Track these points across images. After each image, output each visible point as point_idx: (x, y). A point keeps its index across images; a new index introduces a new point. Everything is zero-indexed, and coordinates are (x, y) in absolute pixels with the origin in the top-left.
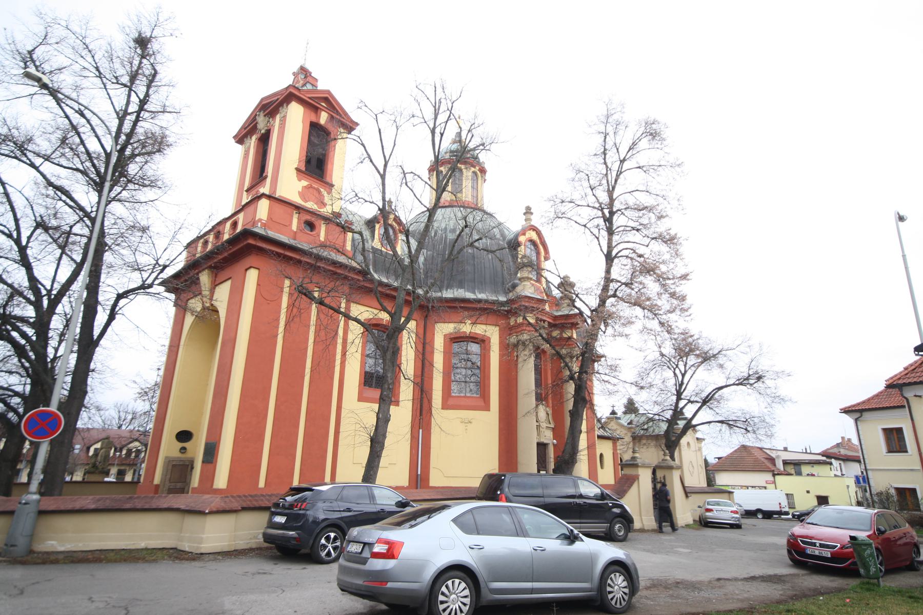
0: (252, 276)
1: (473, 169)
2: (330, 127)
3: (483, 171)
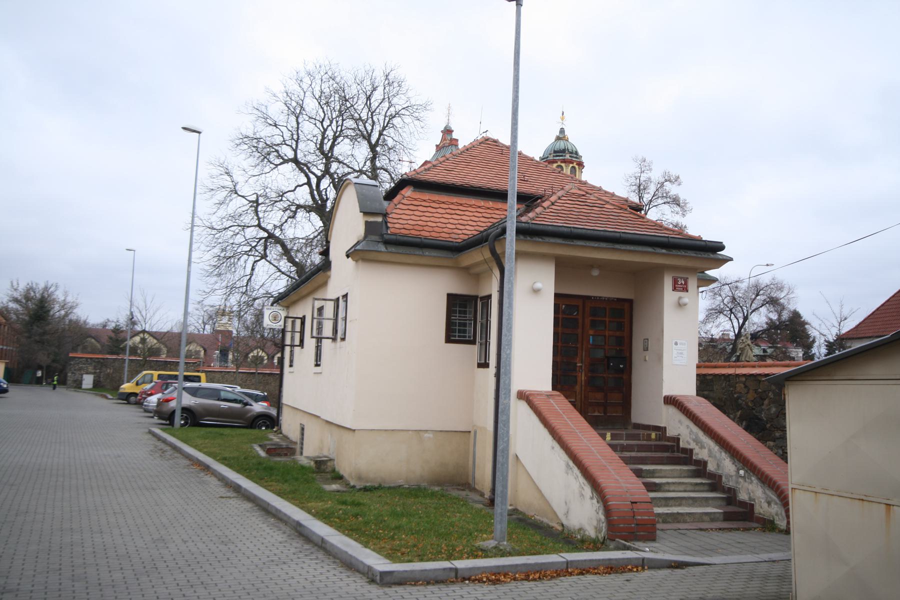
1: (571, 165)
3: (581, 165)
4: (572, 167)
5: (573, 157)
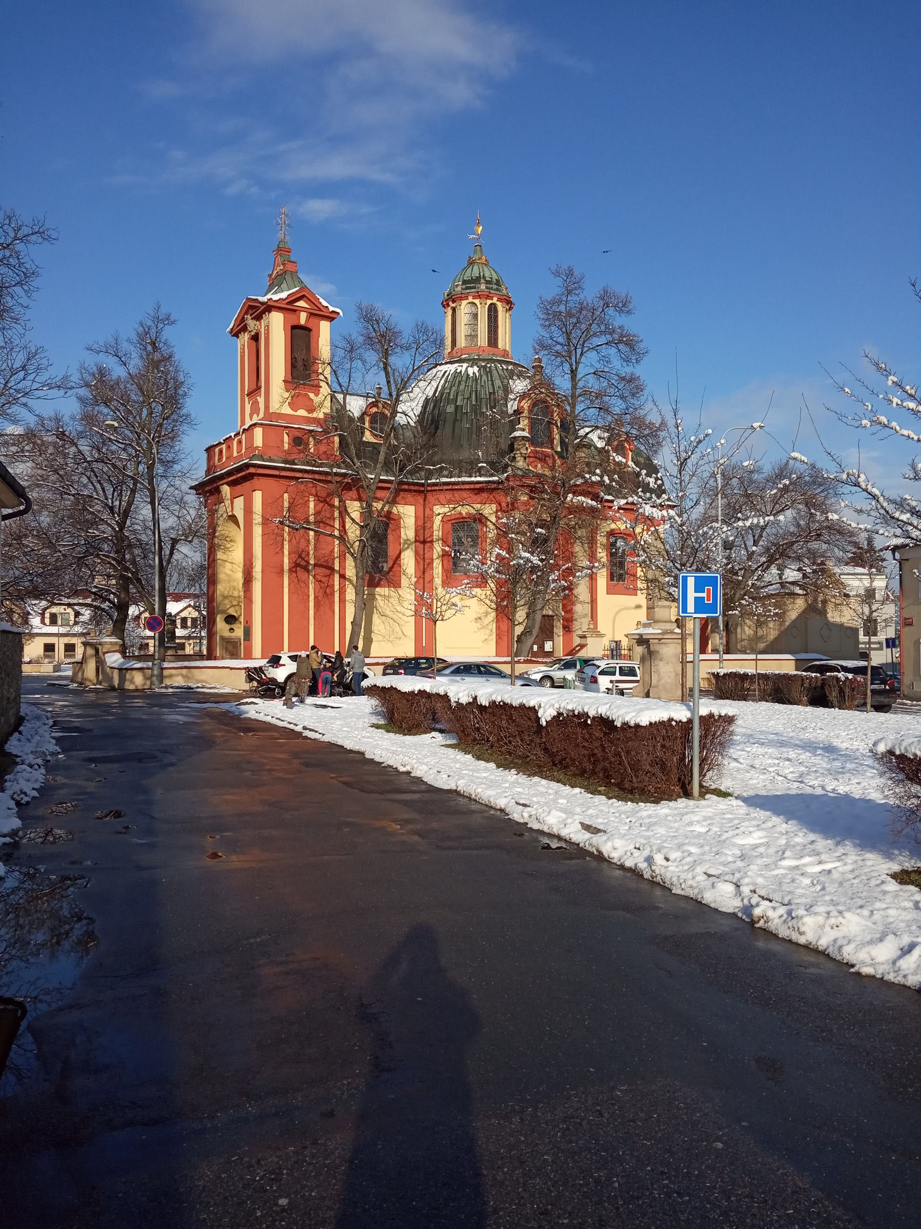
0: (258, 496)
1: (489, 302)
2: (309, 326)
4: (491, 304)
5: (492, 289)
